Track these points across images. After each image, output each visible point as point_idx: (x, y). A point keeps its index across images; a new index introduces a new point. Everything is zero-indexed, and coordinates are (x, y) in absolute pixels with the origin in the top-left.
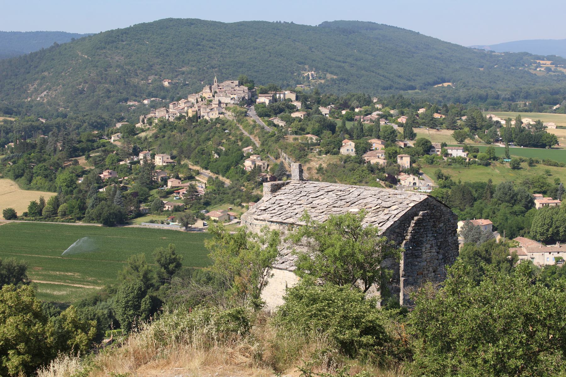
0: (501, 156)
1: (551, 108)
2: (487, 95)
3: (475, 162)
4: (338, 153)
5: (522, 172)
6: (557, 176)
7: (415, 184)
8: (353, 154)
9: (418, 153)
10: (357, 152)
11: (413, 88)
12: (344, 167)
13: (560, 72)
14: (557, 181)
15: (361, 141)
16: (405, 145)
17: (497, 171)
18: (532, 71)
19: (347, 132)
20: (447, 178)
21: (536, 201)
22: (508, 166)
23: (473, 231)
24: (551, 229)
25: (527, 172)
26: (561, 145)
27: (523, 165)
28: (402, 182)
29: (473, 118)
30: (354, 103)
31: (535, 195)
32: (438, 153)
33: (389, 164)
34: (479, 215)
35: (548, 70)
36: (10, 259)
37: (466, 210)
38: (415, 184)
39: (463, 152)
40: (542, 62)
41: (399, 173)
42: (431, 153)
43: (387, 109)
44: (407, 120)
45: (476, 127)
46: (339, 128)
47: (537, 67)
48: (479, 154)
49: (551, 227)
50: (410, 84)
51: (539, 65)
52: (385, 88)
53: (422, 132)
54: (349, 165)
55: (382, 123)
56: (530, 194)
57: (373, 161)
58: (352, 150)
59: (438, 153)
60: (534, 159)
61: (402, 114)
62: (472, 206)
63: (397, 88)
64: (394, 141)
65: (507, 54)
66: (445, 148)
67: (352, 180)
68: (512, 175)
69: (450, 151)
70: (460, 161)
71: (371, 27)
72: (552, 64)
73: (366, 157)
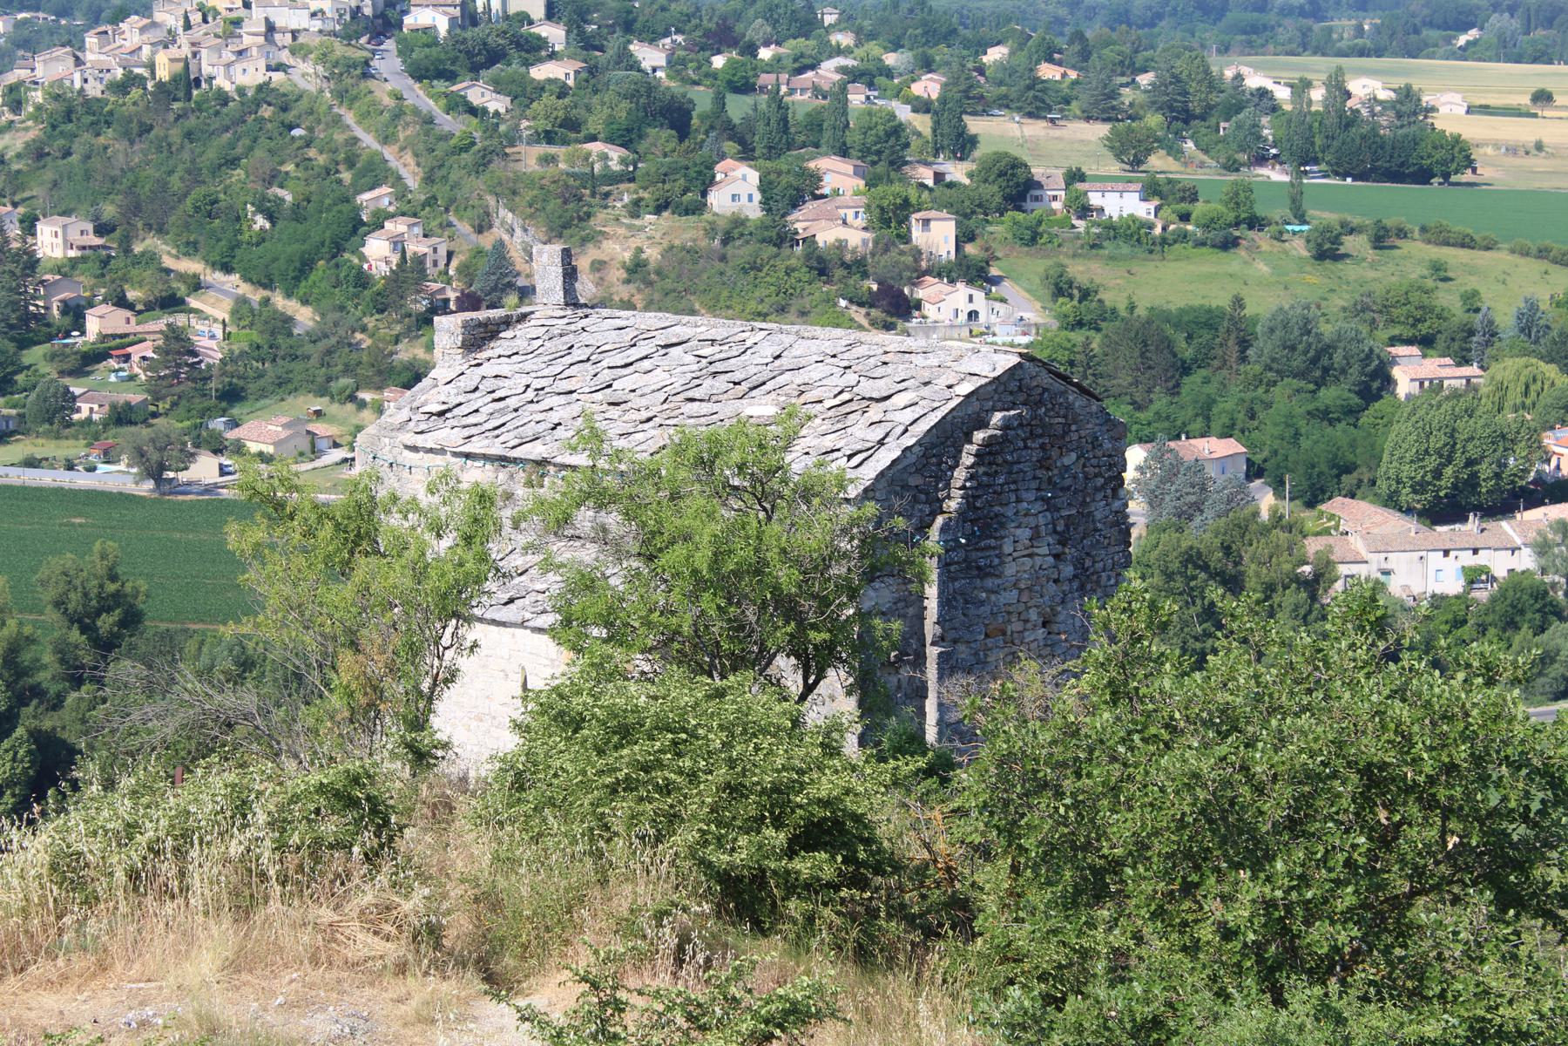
1: (1448, 40)
3: (1183, 237)
4: (698, 208)
5: (1348, 269)
6: (1472, 283)
7: (973, 315)
8: (753, 211)
10: (767, 204)
12: (723, 258)
14: (1471, 301)
15: (782, 164)
16: (939, 177)
17: (1262, 268)
20: (1085, 295)
21: (1396, 372)
22: (1299, 248)
23: (1180, 479)
24: (1449, 471)
27: (1351, 243)
29: (1177, 79)
30: (756, 28)
33: (882, 247)
36: (839, 233)
38: (973, 315)
41: (918, 275)
42: (1029, 205)
43: (873, 48)
44: (944, 86)
45: (1187, 111)
46: (703, 117)
48: (1199, 209)
49: (1450, 460)
54: (741, 252)
56: (1377, 347)
57: (826, 236)
58: (750, 198)
59: (1057, 205)
61: (928, 65)
62: (1174, 390)
64: (898, 163)
66: (1080, 186)
67: (752, 305)
69: (1095, 199)
70: (1131, 233)
73: (801, 221)
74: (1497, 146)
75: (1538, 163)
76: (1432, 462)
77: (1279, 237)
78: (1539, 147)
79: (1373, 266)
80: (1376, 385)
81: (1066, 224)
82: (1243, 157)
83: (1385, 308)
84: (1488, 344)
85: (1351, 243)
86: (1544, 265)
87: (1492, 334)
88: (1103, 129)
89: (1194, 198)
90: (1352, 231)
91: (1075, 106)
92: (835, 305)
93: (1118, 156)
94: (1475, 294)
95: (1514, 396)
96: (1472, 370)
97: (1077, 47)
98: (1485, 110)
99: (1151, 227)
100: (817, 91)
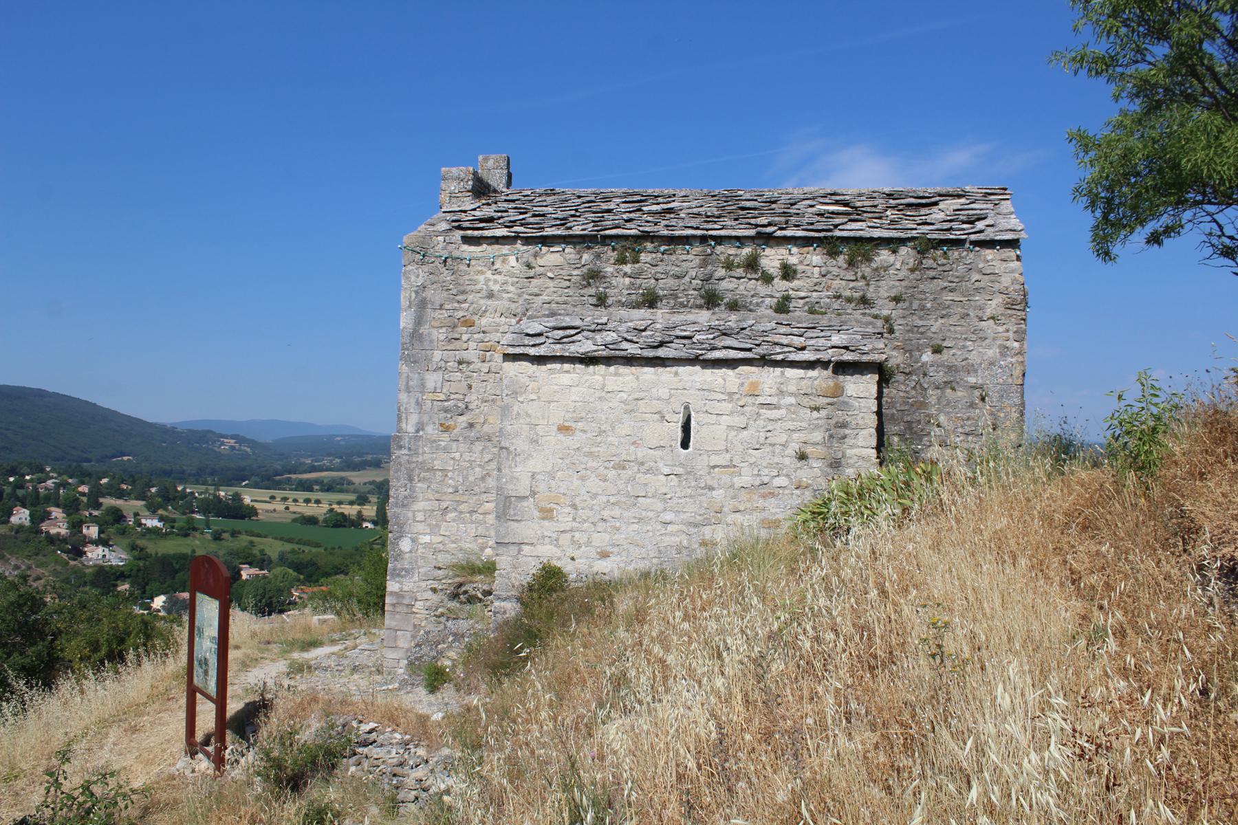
0: (201, 527)
1: (240, 483)
2: (172, 470)
3: (172, 533)
4: (8, 522)
5: (225, 543)
6: (262, 547)
7: (104, 556)
8: (27, 523)
9: (107, 523)
10: (31, 521)
11: (88, 460)
12: (16, 538)
13: (244, 450)
14: (262, 551)
15: (38, 508)
16: (90, 514)
17: (197, 542)
18: (216, 449)
19: (17, 498)
20: (142, 550)
21: (242, 572)
22: (209, 537)
23: (179, 604)
24: (264, 600)
25: (229, 543)
26: (260, 517)
27: (225, 535)
28: (89, 555)
29: (166, 488)
30: (25, 469)
31: (241, 566)
32: (130, 523)
33: (72, 534)
34: (181, 589)
35: (233, 448)
36: (58, 530)
37: (167, 583)
38: (104, 556)
39: (159, 521)
40: (226, 440)
41: (85, 545)
42: (122, 523)
43: (65, 477)
44: (89, 489)
45: (168, 497)
46: (8, 494)
47: (221, 445)
48: (176, 525)
49: (264, 597)
50: (85, 455)
51: (223, 443)
52: (57, 459)
53: (109, 502)
54: (22, 536)
55: (1156, 146)
56: (237, 564)
57: (53, 531)
58: (26, 519)
59: (130, 523)
60: (236, 529)
61: (83, 483)
62: (174, 578)
63: (69, 460)
64: (77, 510)
65: (190, 431)
66: (139, 517)
67: (26, 553)
68: (213, 547)
69: (143, 521)
70: (154, 531)
71: (41, 394)
72: (236, 443)
73: (44, 527)
74: (263, 510)
76: (258, 598)
77: (202, 533)
78: (275, 510)
84: (269, 564)
85: (225, 535)
86: (282, 542)
87: (270, 561)
90: (225, 532)
91: (132, 496)
92: (56, 553)
95: (280, 578)
96: (266, 572)
98: (256, 501)
100: (46, 488)
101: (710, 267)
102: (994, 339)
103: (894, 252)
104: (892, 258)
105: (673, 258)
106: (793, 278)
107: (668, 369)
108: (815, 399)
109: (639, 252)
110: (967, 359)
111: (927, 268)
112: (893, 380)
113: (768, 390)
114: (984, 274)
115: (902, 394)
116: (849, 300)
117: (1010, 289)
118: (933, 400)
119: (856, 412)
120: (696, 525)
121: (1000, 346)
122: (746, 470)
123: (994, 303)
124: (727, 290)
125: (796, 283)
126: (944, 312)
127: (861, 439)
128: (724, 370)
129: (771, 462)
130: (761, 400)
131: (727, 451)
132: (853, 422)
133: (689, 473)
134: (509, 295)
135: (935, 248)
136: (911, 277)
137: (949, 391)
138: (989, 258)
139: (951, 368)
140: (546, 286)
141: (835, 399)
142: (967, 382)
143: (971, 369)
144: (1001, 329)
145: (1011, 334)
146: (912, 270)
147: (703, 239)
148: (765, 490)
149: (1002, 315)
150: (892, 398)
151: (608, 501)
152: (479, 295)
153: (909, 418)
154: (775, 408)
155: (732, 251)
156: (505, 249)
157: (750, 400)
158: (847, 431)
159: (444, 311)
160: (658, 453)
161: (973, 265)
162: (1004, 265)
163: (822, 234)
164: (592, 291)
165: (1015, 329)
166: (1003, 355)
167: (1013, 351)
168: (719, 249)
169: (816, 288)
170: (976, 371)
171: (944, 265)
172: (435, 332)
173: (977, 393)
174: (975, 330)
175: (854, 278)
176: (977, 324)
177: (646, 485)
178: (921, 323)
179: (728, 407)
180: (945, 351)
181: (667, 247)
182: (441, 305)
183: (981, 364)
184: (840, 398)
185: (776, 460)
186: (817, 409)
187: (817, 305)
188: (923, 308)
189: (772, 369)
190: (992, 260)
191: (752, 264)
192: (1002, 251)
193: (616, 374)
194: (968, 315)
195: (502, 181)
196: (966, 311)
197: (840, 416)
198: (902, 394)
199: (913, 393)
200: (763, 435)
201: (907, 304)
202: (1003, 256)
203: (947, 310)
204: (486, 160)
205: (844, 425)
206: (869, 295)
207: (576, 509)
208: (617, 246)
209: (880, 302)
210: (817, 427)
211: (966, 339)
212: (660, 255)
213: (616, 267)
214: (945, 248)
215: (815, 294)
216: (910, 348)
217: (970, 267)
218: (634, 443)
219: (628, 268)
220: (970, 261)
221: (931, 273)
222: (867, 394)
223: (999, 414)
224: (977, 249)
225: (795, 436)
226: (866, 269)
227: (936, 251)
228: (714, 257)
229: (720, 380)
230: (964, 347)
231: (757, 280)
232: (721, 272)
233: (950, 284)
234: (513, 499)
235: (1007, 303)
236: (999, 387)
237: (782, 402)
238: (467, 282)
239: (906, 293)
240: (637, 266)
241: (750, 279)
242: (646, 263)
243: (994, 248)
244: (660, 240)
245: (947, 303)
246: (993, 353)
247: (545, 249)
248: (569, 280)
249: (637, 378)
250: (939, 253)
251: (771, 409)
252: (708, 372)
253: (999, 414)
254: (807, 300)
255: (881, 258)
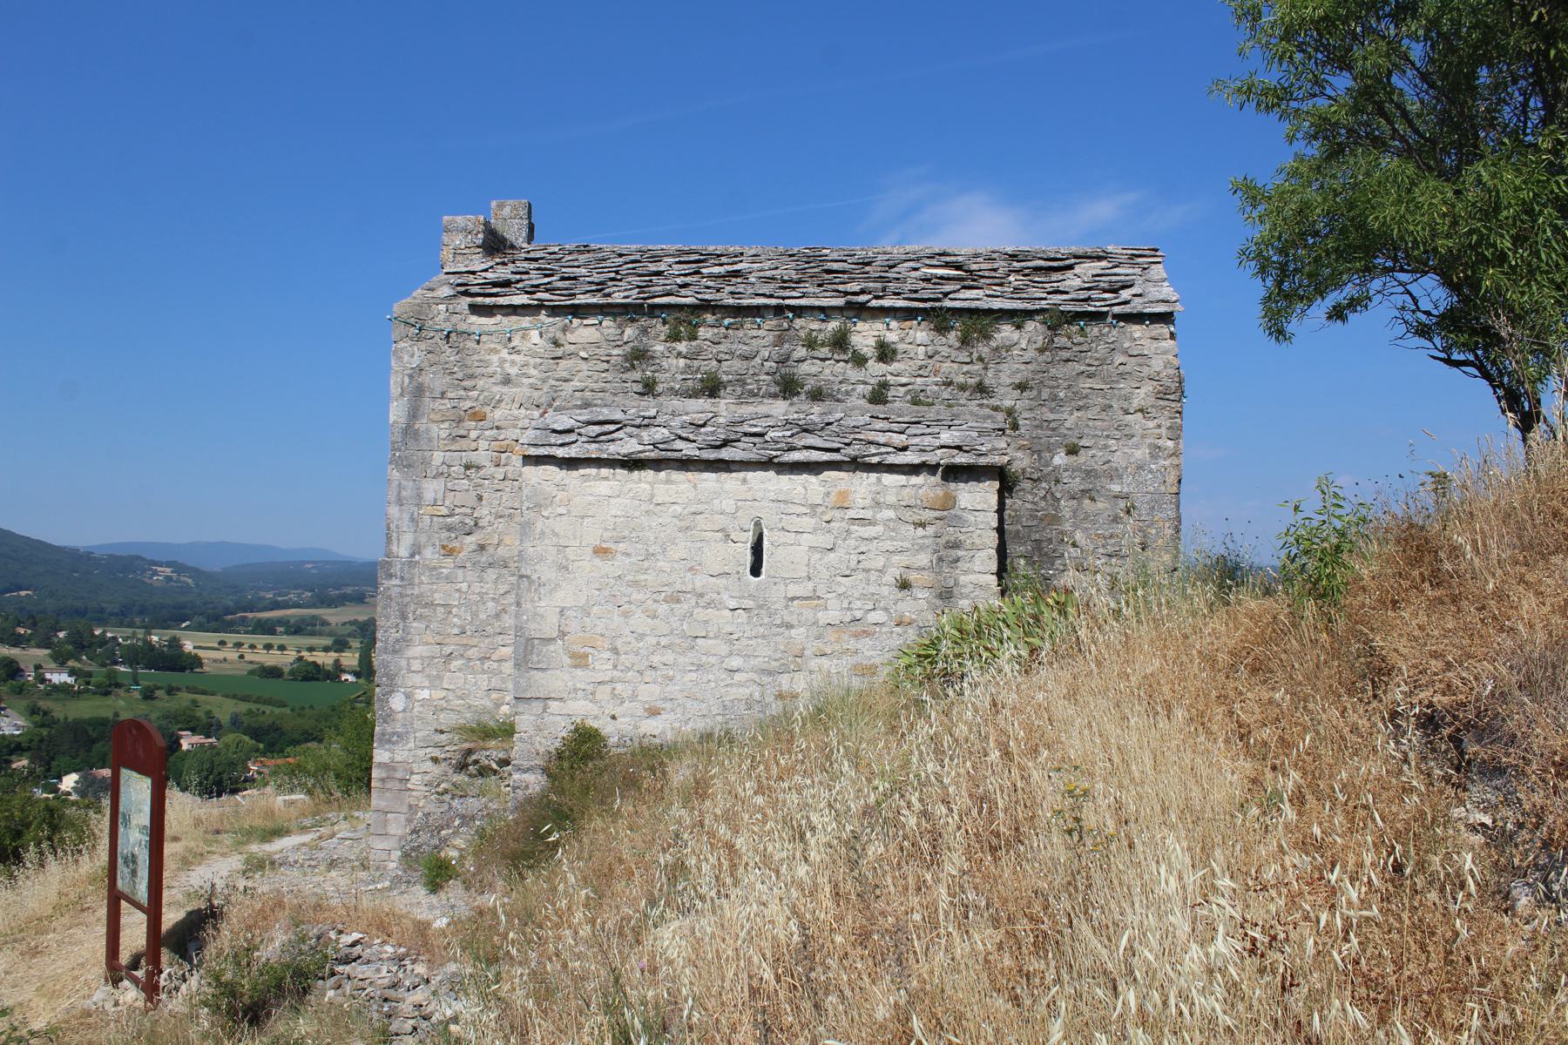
3: (87, 691)
5: (157, 703)
6: (208, 707)
14: (208, 713)
20: (46, 713)
21: (182, 741)
22: (137, 695)
24: (211, 777)
27: (158, 693)
29: (79, 632)
48: (93, 680)
49: (211, 773)
59: (30, 678)
62: (89, 751)
69: (48, 676)
70: (63, 689)
75: (226, 665)
77: (128, 691)
78: (225, 660)
79: (167, 702)
80: (175, 746)
81: (34, 686)
82: (108, 662)
83: (175, 717)
85: (158, 693)
86: (235, 701)
87: (220, 726)
88: (47, 651)
89: (91, 676)
93: (55, 661)
94: (210, 711)
95: (233, 749)
96: (213, 740)
97: (31, 621)
98: (200, 648)
99: (74, 686)
101: (786, 346)
102: (1143, 437)
103: (1019, 327)
104: (1016, 336)
105: (740, 333)
106: (892, 360)
107: (734, 475)
108: (920, 512)
109: (697, 326)
110: (1109, 461)
111: (1060, 348)
112: (1018, 488)
113: (860, 501)
114: (1130, 356)
115: (1028, 506)
116: (963, 388)
117: (1161, 376)
118: (1067, 513)
119: (971, 529)
120: (770, 673)
121: (1150, 446)
122: (833, 603)
123: (1142, 391)
124: (809, 375)
125: (895, 366)
126: (1081, 403)
127: (978, 563)
128: (805, 475)
129: (865, 592)
130: (851, 514)
131: (809, 579)
132: (968, 542)
133: (760, 607)
134: (531, 381)
135: (1069, 323)
136: (1040, 359)
137: (1087, 501)
138: (1137, 335)
139: (1089, 474)
140: (578, 369)
141: (945, 513)
142: (1109, 490)
143: (1114, 475)
144: (1151, 424)
145: (1163, 431)
146: (1041, 351)
147: (779, 310)
148: (859, 628)
149: (1152, 406)
150: (1016, 511)
151: (658, 644)
152: (493, 380)
153: (1037, 536)
154: (870, 524)
155: (815, 325)
156: (526, 321)
157: (838, 514)
158: (960, 553)
159: (447, 401)
160: (722, 581)
161: (1116, 344)
162: (1155, 344)
163: (928, 305)
164: (637, 375)
165: (1169, 425)
166: (1154, 457)
167: (1166, 452)
168: (798, 323)
169: (921, 372)
170: (1120, 477)
171: (1080, 344)
172: (434, 428)
173: (1122, 504)
174: (1120, 426)
175: (968, 360)
176: (1121, 417)
177: (707, 622)
178: (1052, 417)
179: (807, 523)
180: (1082, 451)
181: (732, 320)
182: (443, 393)
183: (1127, 468)
184: (952, 511)
185: (872, 589)
186: (922, 525)
187: (922, 394)
188: (1054, 398)
189: (865, 474)
190: (1140, 338)
191: (840, 342)
192: (1152, 327)
193: (668, 482)
194: (1112, 406)
195: (521, 233)
196: (1108, 402)
197: (951, 533)
198: (1028, 506)
199: (1043, 504)
200: (854, 558)
201: (1035, 393)
202: (1154, 333)
203: (1085, 400)
204: (501, 207)
205: (956, 545)
206: (987, 382)
207: (617, 654)
208: (669, 319)
209: (1001, 390)
210: (922, 548)
211: (1108, 436)
212: (723, 330)
213: (668, 345)
214: (1082, 323)
215: (919, 380)
216: (1039, 447)
217: (1112, 346)
218: (691, 569)
219: (682, 347)
220: (1113, 339)
221: (1065, 354)
222: (985, 507)
223: (1149, 530)
224: (1122, 324)
225: (896, 558)
226: (983, 349)
227: (1071, 327)
228: (792, 332)
229: (800, 489)
230: (1106, 447)
231: (846, 362)
232: (801, 352)
233: (1089, 368)
234: (536, 642)
235: (1159, 392)
236: (1149, 496)
237: (878, 516)
238: (477, 364)
239: (1033, 379)
240: (694, 343)
241: (838, 361)
242: (706, 340)
243: (1143, 323)
244: (723, 311)
245: (1085, 391)
246: (1141, 454)
247: (576, 322)
248: (608, 362)
249: (695, 486)
250: (1075, 328)
251: (864, 526)
252: (785, 478)
253: (1149, 530)
254: (910, 387)
255: (1002, 334)
